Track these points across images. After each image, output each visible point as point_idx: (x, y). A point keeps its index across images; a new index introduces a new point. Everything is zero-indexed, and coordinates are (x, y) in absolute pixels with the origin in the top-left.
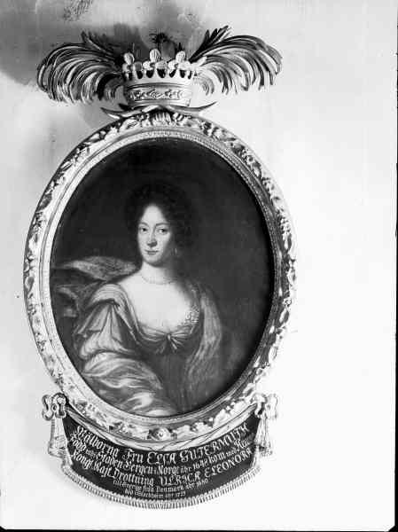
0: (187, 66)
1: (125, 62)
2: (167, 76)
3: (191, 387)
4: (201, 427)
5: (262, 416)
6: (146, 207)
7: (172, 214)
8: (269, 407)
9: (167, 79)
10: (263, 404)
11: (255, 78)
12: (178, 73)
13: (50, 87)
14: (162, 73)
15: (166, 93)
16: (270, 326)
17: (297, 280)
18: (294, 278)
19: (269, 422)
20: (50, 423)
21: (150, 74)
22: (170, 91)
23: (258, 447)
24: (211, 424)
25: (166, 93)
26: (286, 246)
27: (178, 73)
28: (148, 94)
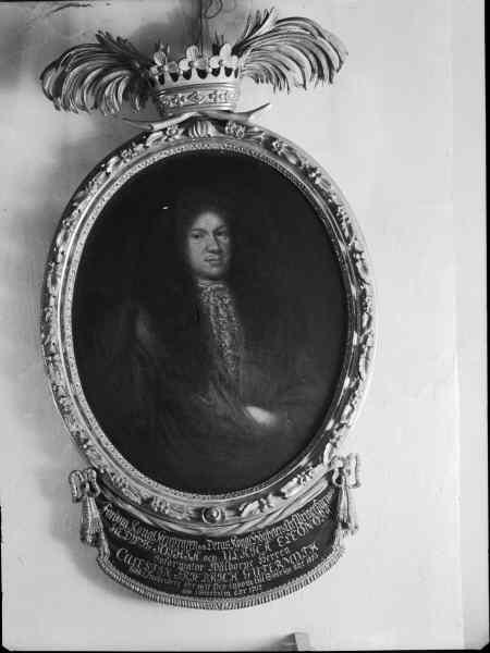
0: (233, 62)
1: (155, 64)
2: (181, 78)
3: (259, 415)
4: (273, 500)
5: (343, 486)
6: (211, 210)
7: (233, 227)
8: (349, 472)
9: (210, 79)
10: (340, 469)
11: (109, 82)
12: (223, 71)
13: (55, 95)
14: (203, 74)
15: (210, 96)
16: (344, 379)
17: (370, 271)
18: (365, 269)
19: (353, 492)
20: (81, 504)
21: (187, 75)
22: (215, 93)
23: (340, 524)
24: (282, 495)
25: (210, 96)
26: (347, 234)
27: (223, 71)
28: (188, 98)
